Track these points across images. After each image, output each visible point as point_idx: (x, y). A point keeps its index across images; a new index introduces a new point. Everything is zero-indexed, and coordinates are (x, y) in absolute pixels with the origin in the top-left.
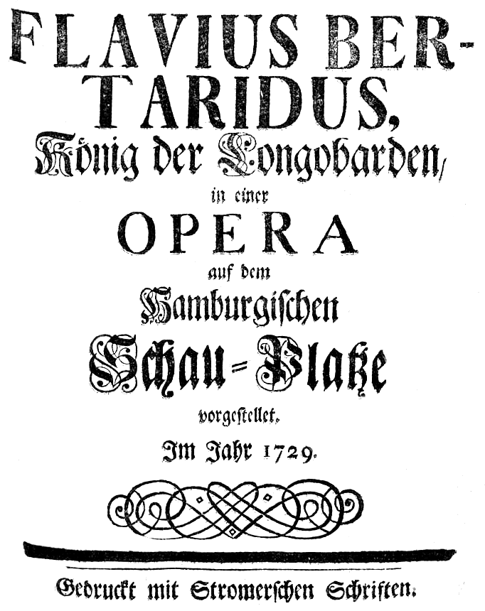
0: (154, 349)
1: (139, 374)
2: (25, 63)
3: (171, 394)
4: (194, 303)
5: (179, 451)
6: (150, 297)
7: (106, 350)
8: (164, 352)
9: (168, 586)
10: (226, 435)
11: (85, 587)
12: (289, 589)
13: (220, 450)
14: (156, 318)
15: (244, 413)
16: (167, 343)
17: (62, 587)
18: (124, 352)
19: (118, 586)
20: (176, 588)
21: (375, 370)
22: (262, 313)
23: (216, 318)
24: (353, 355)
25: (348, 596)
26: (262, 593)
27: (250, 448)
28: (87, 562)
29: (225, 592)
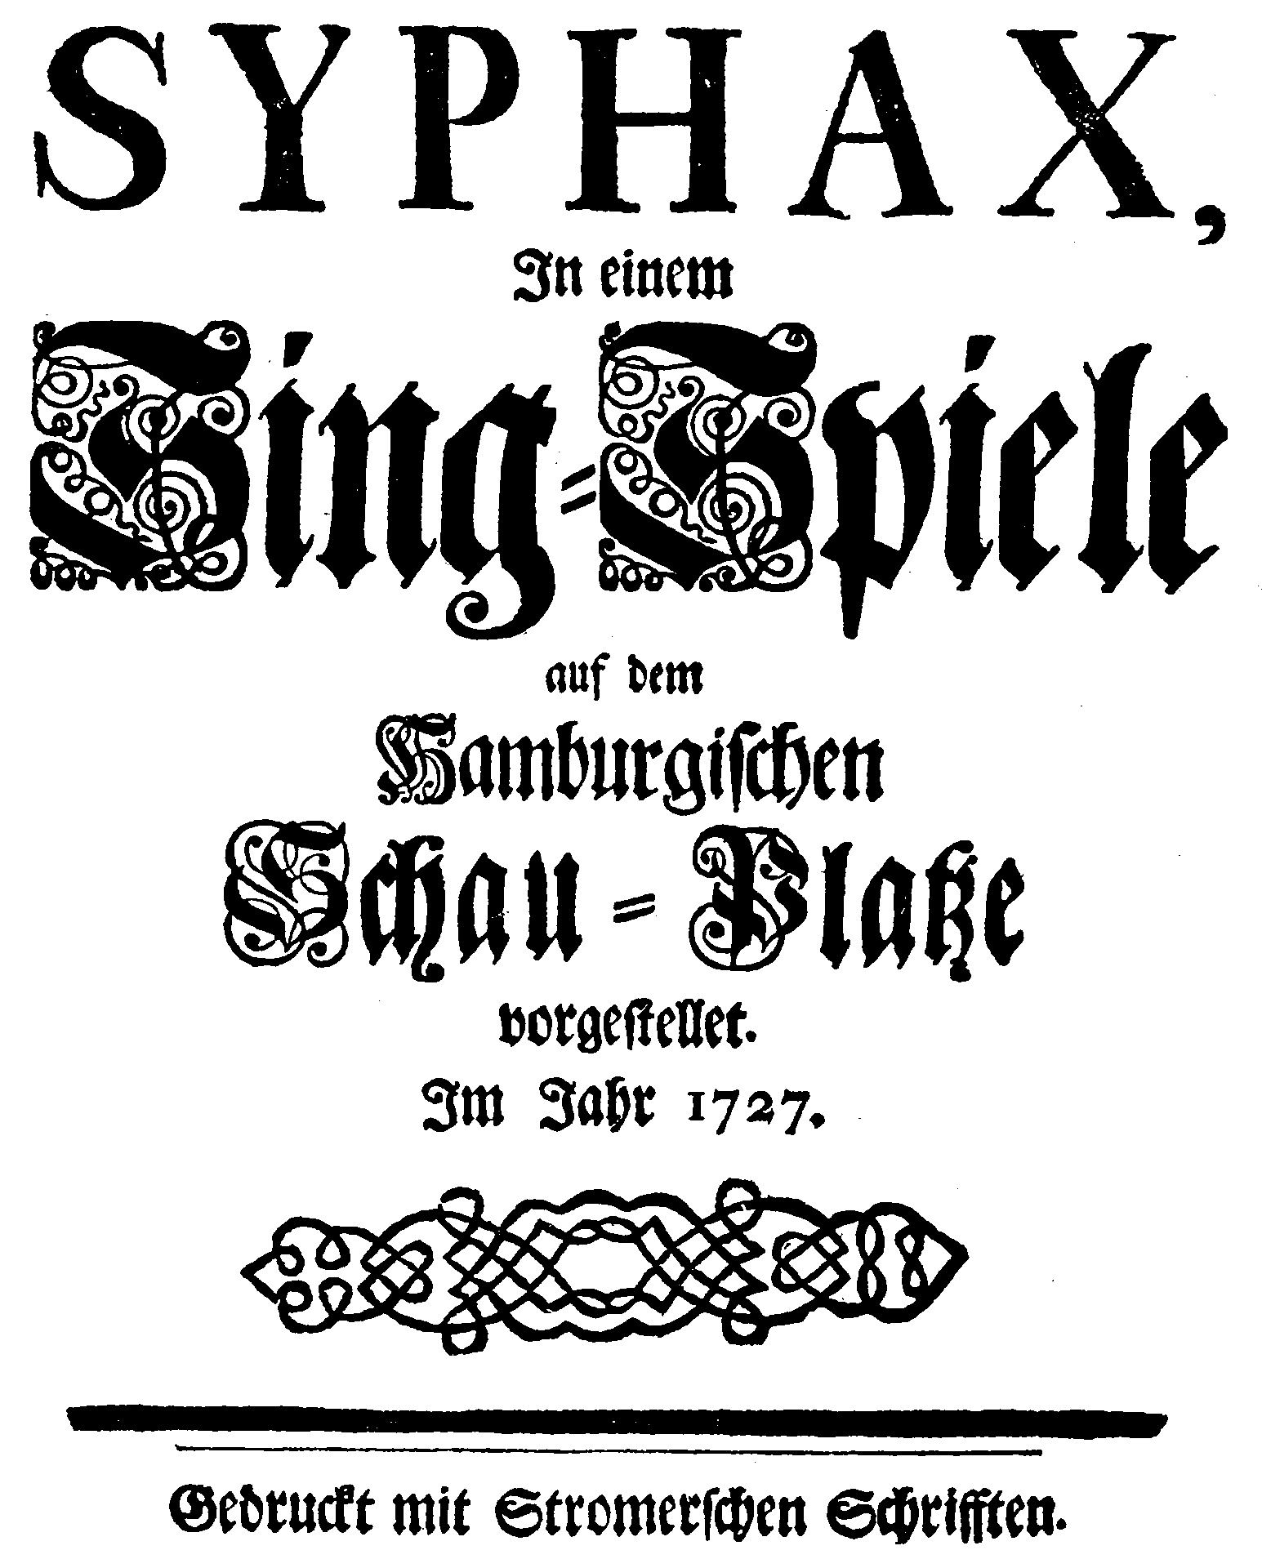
0: (393, 861)
1: (353, 918)
2: (1213, 549)
3: (436, 973)
4: (515, 756)
5: (465, 1104)
6: (404, 736)
7: (268, 855)
8: (418, 866)
9: (444, 1502)
10: (588, 1071)
11: (244, 1506)
12: (743, 1509)
13: (575, 1100)
14: (419, 791)
15: (646, 1017)
16: (426, 845)
17: (185, 1507)
18: (314, 864)
19: (329, 1499)
20: (368, 1508)
21: (996, 909)
22: (685, 781)
23: (570, 791)
24: (938, 874)
25: (885, 1530)
26: (674, 1518)
27: (650, 1098)
28: (539, 1435)
29: (581, 1516)
